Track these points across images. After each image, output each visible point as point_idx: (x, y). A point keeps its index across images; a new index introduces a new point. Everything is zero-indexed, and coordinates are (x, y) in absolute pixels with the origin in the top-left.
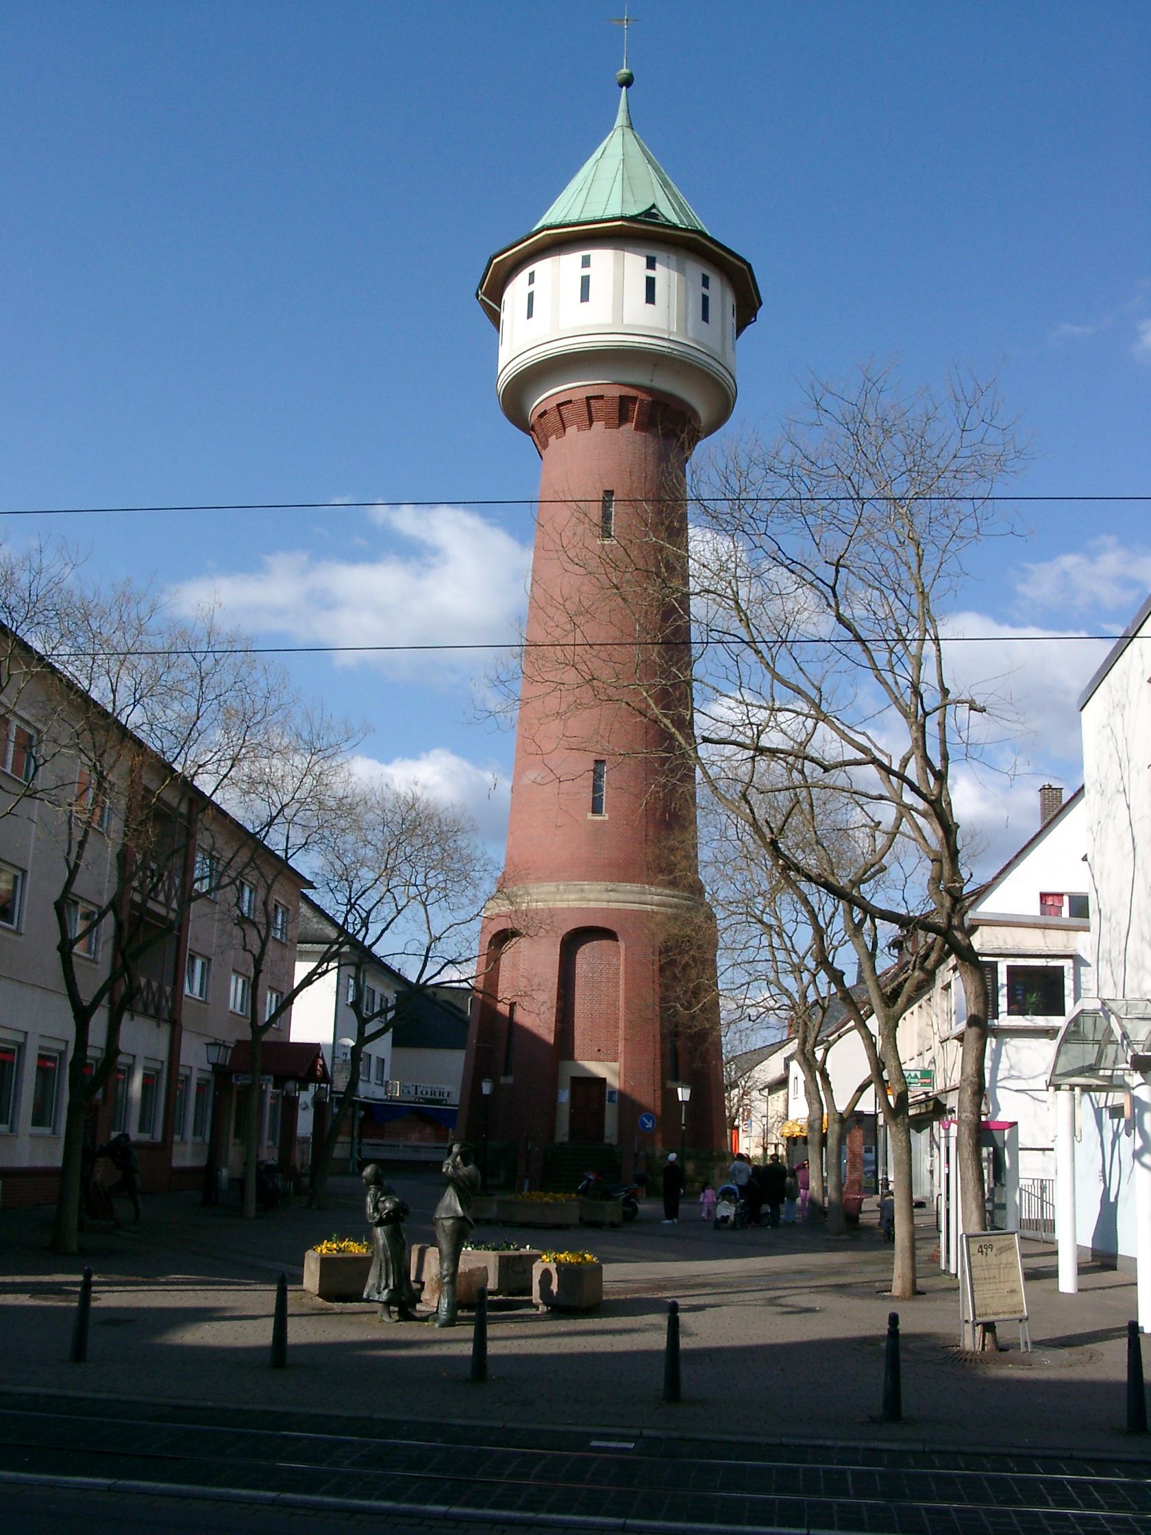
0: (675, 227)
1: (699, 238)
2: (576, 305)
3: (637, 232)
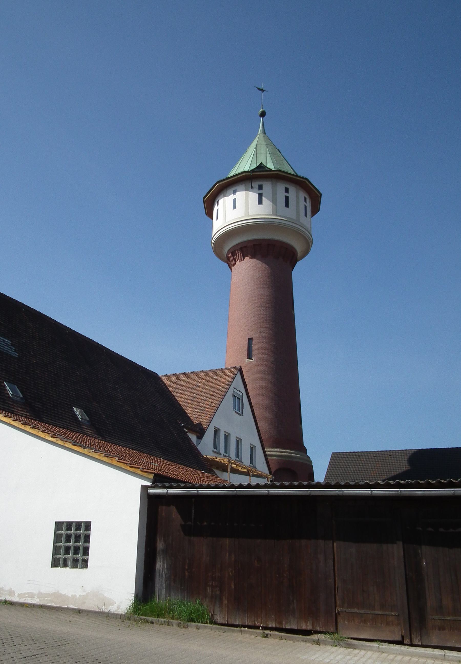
0: (271, 170)
1: (246, 174)
2: (236, 210)
3: (256, 178)
